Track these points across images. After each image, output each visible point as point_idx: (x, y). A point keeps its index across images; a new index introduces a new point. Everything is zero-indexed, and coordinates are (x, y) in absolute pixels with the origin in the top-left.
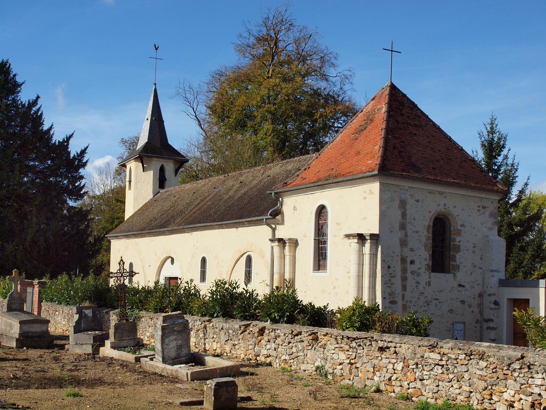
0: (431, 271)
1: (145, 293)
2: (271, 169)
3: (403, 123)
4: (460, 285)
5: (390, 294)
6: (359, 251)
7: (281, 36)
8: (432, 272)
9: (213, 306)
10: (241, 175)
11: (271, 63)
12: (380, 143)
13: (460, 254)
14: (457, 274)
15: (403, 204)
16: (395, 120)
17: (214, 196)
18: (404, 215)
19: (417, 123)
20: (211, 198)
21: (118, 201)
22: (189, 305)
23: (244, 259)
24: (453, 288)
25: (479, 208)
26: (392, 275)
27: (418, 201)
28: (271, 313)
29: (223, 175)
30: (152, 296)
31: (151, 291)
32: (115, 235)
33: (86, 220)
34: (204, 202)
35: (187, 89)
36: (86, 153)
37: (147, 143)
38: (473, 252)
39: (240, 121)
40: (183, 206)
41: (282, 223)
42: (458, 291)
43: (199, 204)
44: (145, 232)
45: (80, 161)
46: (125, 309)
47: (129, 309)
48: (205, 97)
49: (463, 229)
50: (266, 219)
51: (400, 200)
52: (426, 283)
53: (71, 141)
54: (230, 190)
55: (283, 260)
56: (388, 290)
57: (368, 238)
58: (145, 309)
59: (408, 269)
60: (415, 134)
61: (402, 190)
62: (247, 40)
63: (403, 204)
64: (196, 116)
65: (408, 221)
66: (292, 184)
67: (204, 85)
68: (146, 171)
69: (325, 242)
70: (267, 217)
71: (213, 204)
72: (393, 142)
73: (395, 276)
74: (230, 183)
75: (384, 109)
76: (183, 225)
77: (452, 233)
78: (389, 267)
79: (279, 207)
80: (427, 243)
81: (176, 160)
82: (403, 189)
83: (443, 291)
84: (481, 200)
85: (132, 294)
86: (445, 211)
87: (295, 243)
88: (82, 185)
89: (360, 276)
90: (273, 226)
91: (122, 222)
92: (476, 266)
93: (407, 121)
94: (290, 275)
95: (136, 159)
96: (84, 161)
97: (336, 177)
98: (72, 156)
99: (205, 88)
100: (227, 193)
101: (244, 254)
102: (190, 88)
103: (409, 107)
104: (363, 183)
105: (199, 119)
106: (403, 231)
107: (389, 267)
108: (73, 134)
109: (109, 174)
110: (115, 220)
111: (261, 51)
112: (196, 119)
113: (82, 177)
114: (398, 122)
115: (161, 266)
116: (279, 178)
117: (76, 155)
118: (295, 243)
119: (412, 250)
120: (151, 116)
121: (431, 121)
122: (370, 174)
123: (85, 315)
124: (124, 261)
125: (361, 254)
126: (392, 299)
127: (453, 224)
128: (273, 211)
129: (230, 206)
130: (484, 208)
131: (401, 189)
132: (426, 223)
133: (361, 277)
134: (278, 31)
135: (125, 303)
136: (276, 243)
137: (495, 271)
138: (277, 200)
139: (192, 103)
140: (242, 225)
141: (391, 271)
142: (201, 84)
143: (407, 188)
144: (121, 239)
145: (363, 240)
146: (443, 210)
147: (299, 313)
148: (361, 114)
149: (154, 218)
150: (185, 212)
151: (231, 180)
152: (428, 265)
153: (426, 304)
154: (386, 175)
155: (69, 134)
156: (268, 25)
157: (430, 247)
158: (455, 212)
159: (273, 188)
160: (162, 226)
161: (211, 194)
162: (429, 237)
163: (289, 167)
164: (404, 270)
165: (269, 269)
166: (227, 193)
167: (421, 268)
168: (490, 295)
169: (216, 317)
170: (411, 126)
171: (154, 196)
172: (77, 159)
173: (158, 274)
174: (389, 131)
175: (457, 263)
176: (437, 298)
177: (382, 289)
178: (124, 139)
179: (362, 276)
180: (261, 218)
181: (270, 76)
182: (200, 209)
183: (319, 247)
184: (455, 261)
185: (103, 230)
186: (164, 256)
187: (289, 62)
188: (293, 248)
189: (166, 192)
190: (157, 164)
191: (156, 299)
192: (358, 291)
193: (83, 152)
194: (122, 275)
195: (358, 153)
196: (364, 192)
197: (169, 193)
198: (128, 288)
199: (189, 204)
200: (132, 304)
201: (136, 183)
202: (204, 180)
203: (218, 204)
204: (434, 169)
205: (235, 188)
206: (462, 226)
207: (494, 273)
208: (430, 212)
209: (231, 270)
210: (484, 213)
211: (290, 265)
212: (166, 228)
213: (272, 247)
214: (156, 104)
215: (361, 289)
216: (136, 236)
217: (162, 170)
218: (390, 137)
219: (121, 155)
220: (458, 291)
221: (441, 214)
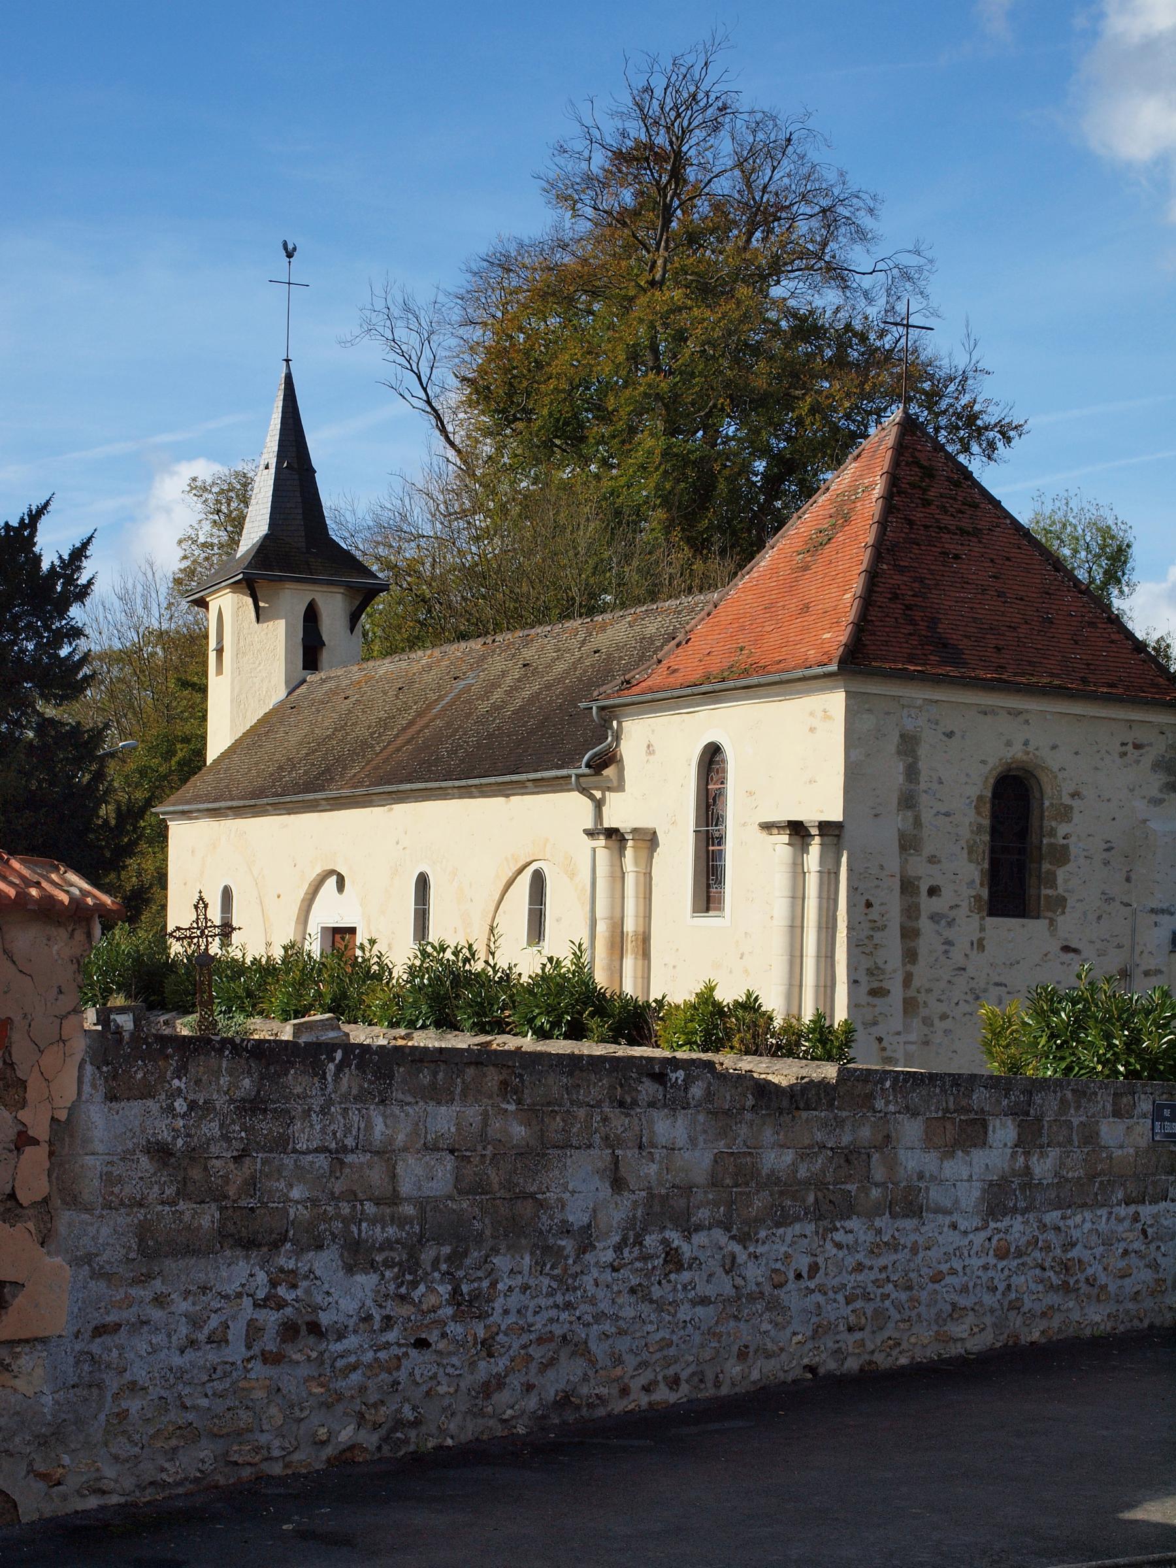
0: (985, 914)
1: (260, 973)
2: (605, 630)
3: (926, 527)
4: (1066, 949)
5: (870, 972)
6: (794, 864)
7: (690, 148)
8: (991, 914)
9: (415, 1005)
10: (527, 642)
11: (662, 235)
12: (857, 585)
13: (1067, 868)
14: (1060, 919)
15: (908, 744)
16: (905, 519)
17: (452, 703)
18: (912, 773)
19: (966, 524)
20: (444, 709)
21: (185, 684)
22: (362, 1002)
23: (524, 883)
24: (1046, 955)
25: (1124, 749)
26: (877, 924)
27: (950, 735)
28: (535, 1017)
29: (481, 640)
30: (278, 981)
31: (275, 969)
32: (180, 808)
33: (93, 758)
34: (425, 720)
35: (396, 312)
36: (86, 557)
37: (266, 537)
38: (1105, 864)
39: (566, 423)
40: (370, 727)
41: (620, 787)
42: (1063, 963)
43: (411, 723)
44: (265, 800)
45: (70, 580)
46: (212, 1011)
47: (221, 1012)
48: (453, 342)
49: (1075, 803)
50: (578, 776)
51: (902, 736)
52: (972, 944)
53: (42, 525)
54: (495, 685)
55: (619, 886)
56: (866, 963)
57: (814, 831)
58: (261, 1013)
59: (922, 907)
60: (957, 557)
61: (905, 710)
62: (584, 165)
63: (908, 744)
64: (429, 402)
65: (923, 786)
66: (643, 684)
67: (452, 305)
68: (264, 622)
69: (720, 840)
70: (579, 771)
71: (449, 725)
72: (890, 581)
73: (885, 926)
74: (497, 664)
75: (878, 491)
76: (368, 786)
77: (1046, 814)
78: (869, 905)
79: (610, 746)
80: (975, 842)
81: (351, 587)
82: (909, 706)
83: (1018, 963)
84: (1130, 727)
85: (227, 976)
86: (1025, 758)
87: (649, 840)
88: (77, 657)
89: (796, 928)
90: (598, 794)
91: (200, 769)
92: (1113, 899)
93: (938, 520)
94: (637, 925)
95: (236, 586)
96: (83, 580)
97: (746, 672)
98: (45, 566)
99: (456, 315)
100: (486, 695)
101: (520, 871)
102: (407, 309)
103: (949, 479)
104: (822, 690)
105: (438, 407)
106: (909, 813)
107: (869, 905)
108: (47, 504)
109: (154, 595)
110: (179, 746)
111: (627, 197)
112: (428, 409)
113: (76, 633)
114: (911, 523)
115: (309, 897)
116: (621, 658)
117: (57, 563)
118: (649, 840)
119: (933, 860)
120: (278, 456)
121: (1008, 515)
122: (819, 670)
123: (118, 1026)
124: (207, 900)
125: (798, 872)
126: (876, 985)
127: (1048, 791)
128: (595, 755)
129: (490, 736)
130: (1137, 746)
131: (903, 706)
132: (974, 791)
133: (799, 930)
134: (683, 132)
135: (211, 997)
136: (601, 841)
137: (1163, 911)
138: (605, 724)
139: (414, 358)
140: (520, 788)
141: (874, 914)
142: (442, 298)
143: (920, 702)
144: (197, 818)
145: (803, 837)
146: (1020, 756)
147: (592, 1015)
148: (823, 497)
149: (289, 759)
150: (372, 747)
151: (499, 655)
152: (978, 898)
153: (970, 998)
154: (860, 673)
155: (36, 504)
156: (650, 113)
157: (984, 852)
158: (1053, 761)
159: (596, 693)
160: (309, 787)
161: (446, 695)
162: (980, 827)
163: (652, 627)
164: (911, 912)
165: (588, 908)
166: (486, 695)
167: (957, 906)
168: (1147, 974)
169: (421, 1028)
170: (949, 533)
171: (289, 694)
172: (59, 576)
173: (303, 918)
174: (882, 551)
175: (1060, 891)
176: (1004, 981)
177: (848, 959)
178: (200, 479)
179: (802, 927)
180: (564, 772)
181: (658, 277)
182: (413, 738)
183: (708, 851)
184: (1051, 887)
185: (142, 777)
186: (318, 870)
187: (721, 225)
188: (644, 854)
189: (323, 681)
190: (294, 598)
191: (286, 987)
192: (791, 964)
193: (79, 554)
194: (202, 932)
195: (805, 609)
196: (812, 714)
197: (330, 685)
198: (219, 961)
199: (384, 723)
200: (229, 999)
201: (237, 654)
202: (429, 652)
203: (460, 727)
204: (998, 649)
205: (509, 680)
206: (1075, 795)
207: (1161, 916)
208: (983, 762)
209: (493, 909)
210: (1138, 762)
211: (637, 897)
212: (320, 791)
213: (594, 850)
214: (291, 421)
215: (798, 960)
216: (238, 812)
217: (311, 616)
218: (885, 567)
219: (192, 533)
220: (1063, 963)
221: (1014, 766)
